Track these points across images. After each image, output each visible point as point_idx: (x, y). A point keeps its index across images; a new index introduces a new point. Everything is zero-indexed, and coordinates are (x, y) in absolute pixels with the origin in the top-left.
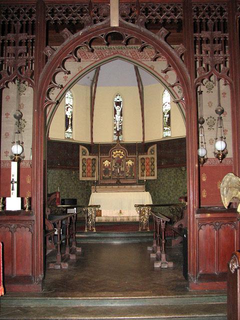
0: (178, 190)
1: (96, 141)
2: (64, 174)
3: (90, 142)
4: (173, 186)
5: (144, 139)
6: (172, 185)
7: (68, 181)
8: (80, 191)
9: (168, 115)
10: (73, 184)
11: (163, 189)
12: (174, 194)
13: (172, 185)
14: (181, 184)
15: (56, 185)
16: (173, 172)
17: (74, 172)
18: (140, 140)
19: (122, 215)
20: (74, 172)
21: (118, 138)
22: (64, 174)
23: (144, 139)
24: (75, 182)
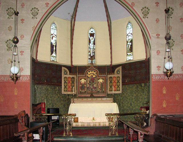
0: (139, 102)
1: (75, 64)
2: (49, 89)
3: (70, 64)
4: (134, 98)
5: (111, 62)
6: (133, 97)
7: (53, 95)
8: (62, 102)
9: (131, 43)
10: (56, 97)
11: (126, 101)
12: (135, 105)
13: (133, 97)
14: (140, 97)
15: (43, 97)
16: (134, 87)
17: (57, 88)
18: (108, 63)
19: (94, 122)
20: (57, 88)
21: (92, 62)
22: (49, 89)
23: (111, 62)
24: (59, 95)
